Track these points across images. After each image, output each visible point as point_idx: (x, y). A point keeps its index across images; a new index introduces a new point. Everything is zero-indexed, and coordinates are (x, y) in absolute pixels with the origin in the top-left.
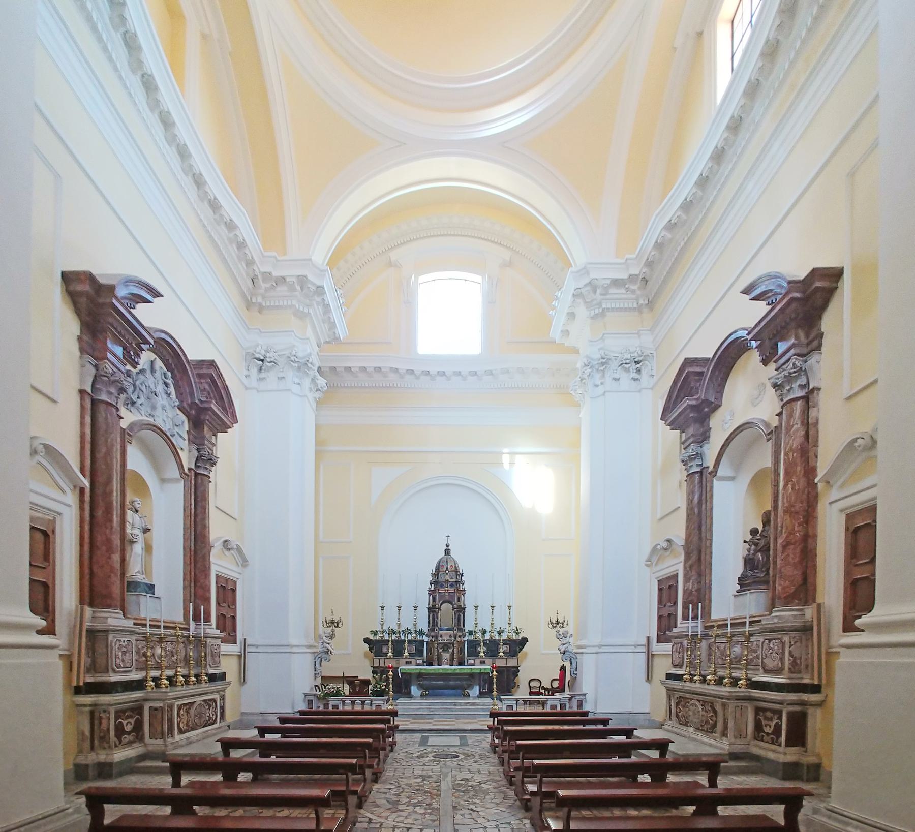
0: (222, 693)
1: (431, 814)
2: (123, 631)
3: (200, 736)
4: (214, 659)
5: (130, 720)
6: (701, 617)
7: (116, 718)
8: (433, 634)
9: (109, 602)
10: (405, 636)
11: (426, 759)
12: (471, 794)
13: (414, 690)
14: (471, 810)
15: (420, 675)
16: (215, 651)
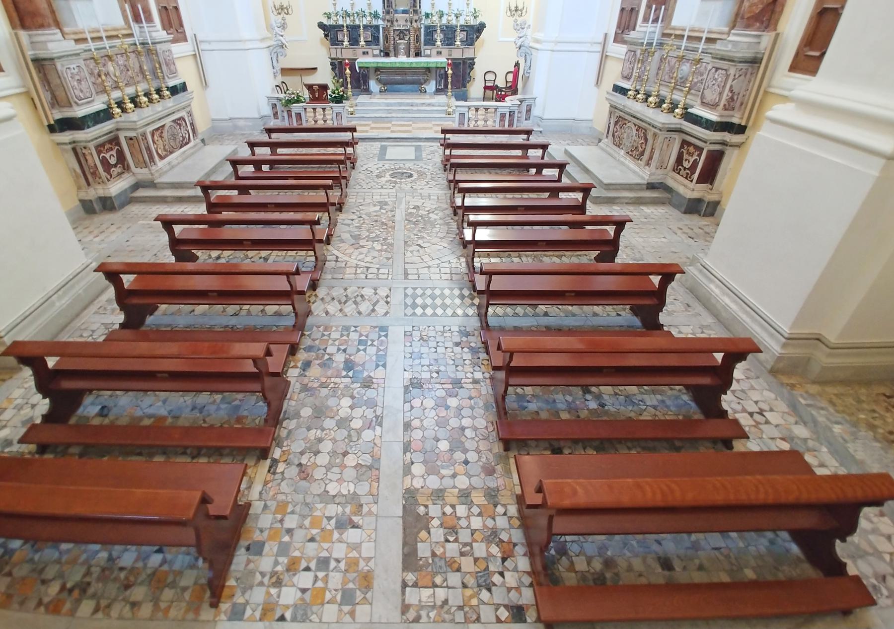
0: (188, 109)
1: (386, 251)
2: (68, 56)
3: (180, 159)
4: (170, 69)
5: (112, 153)
6: (662, 21)
7: (99, 153)
8: (388, 17)
9: (40, 20)
10: (359, 20)
11: (383, 179)
12: (421, 226)
13: (373, 85)
14: (419, 245)
15: (377, 69)
16: (168, 58)
